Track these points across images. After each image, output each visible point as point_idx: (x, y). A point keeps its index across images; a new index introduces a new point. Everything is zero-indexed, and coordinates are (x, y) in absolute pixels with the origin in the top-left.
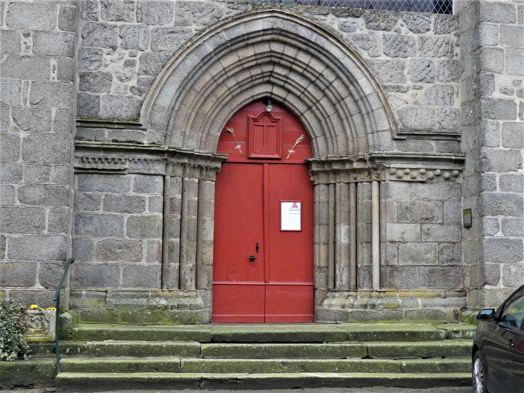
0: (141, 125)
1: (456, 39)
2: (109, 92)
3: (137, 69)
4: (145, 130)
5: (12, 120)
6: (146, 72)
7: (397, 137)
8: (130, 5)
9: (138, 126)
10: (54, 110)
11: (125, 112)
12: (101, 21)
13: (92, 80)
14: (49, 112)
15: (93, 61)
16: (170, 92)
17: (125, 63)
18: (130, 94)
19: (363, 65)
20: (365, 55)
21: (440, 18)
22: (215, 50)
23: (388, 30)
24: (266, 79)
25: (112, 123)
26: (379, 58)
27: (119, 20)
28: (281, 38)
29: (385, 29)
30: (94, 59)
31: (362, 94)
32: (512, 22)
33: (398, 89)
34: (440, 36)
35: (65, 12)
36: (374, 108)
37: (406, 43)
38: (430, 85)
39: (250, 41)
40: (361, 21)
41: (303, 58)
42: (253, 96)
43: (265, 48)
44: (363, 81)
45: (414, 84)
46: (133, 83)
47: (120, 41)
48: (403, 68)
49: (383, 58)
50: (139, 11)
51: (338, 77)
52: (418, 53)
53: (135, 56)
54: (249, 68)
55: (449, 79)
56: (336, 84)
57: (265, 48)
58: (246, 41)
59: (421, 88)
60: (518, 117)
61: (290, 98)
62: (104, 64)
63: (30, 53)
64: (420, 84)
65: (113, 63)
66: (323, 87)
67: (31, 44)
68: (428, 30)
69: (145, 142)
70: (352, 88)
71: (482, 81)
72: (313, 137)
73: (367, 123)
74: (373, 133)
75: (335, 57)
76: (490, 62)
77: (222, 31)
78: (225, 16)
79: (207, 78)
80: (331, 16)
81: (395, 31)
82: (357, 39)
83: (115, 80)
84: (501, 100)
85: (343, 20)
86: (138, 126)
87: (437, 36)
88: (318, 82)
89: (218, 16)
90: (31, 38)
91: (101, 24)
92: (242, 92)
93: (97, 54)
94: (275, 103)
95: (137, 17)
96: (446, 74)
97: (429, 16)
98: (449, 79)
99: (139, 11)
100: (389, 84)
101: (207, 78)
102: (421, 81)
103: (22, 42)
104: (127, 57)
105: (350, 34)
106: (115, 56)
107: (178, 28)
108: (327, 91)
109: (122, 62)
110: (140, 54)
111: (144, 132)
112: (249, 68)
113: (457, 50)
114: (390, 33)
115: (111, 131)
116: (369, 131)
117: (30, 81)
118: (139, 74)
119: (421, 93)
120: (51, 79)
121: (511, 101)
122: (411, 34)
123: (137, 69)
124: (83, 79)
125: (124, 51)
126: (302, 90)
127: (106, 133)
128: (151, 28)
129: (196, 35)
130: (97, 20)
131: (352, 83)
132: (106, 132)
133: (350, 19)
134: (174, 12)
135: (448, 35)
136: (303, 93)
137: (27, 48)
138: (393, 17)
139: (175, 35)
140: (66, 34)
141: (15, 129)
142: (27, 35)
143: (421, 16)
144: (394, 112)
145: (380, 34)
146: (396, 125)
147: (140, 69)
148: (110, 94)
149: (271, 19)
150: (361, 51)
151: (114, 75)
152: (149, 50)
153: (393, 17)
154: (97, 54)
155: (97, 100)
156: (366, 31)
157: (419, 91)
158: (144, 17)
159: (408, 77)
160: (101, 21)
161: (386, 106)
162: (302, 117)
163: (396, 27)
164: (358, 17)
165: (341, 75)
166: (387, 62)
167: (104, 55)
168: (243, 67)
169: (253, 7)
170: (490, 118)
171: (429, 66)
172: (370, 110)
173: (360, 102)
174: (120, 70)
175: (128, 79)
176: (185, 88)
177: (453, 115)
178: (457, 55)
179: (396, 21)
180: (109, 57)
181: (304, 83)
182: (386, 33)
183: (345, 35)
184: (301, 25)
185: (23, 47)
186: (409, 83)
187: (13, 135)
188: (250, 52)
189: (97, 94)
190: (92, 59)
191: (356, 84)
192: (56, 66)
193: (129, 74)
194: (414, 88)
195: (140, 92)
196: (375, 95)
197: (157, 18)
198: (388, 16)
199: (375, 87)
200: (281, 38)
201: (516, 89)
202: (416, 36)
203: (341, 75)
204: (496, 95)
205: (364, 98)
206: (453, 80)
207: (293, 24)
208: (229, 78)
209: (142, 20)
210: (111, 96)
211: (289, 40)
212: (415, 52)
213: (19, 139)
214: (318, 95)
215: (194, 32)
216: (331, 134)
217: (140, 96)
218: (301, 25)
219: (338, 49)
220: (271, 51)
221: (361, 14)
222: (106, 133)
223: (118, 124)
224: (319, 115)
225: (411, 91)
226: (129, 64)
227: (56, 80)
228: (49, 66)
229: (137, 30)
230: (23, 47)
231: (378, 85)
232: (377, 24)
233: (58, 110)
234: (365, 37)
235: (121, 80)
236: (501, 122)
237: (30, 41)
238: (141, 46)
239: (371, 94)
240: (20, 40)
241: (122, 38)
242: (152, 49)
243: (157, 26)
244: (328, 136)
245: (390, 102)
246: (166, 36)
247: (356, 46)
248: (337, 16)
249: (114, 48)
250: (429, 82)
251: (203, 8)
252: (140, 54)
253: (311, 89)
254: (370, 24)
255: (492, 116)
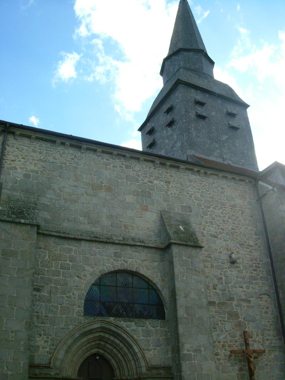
0: (51, 367)
1: (168, 330)
2: (38, 353)
3: (49, 343)
4: (53, 369)
5: (5, 367)
6: (53, 345)
7: (148, 369)
8: (47, 318)
9: (49, 367)
10: (22, 362)
11: (44, 362)
12: (36, 324)
13: (32, 348)
14: (20, 363)
15: (33, 340)
16: (62, 353)
17: (45, 341)
18: (46, 354)
19: (135, 340)
20: (135, 337)
21: (162, 322)
22: (79, 336)
23: (144, 327)
24: (97, 346)
25: (40, 366)
26: (140, 338)
27: (43, 324)
28: (104, 330)
29: (142, 326)
30: (33, 339)
31: (135, 352)
32: (189, 324)
33: (148, 350)
34: (163, 328)
35: (27, 323)
36: (139, 357)
37: (150, 332)
38: (159, 348)
39: (92, 332)
40: (133, 323)
41: (112, 338)
42: (91, 353)
43: (97, 334)
44: (135, 347)
45: (153, 347)
46: (48, 349)
47: (43, 332)
48: (149, 341)
49: (142, 338)
50: (50, 320)
51: (125, 345)
52: (155, 336)
53: (48, 338)
54: (91, 342)
55: (166, 345)
56: (124, 348)
57: (97, 334)
58: (91, 332)
59: (156, 349)
60: (193, 360)
61: (106, 354)
62: (36, 342)
63: (14, 339)
64: (156, 347)
65: (40, 341)
66: (119, 349)
67: (14, 336)
68: (158, 326)
69: (52, 374)
70: (131, 350)
71: (180, 347)
72: (115, 369)
73: (137, 363)
74: (139, 367)
75: (124, 338)
76: (182, 339)
77: (82, 328)
78: (83, 322)
79: (76, 347)
80: (123, 322)
81: (146, 327)
82: (132, 330)
83: (41, 348)
84: (187, 354)
85: (126, 323)
86: (49, 367)
87: (161, 328)
88: (117, 347)
89: (81, 322)
90: (14, 333)
91: (36, 326)
92: (87, 351)
93: (34, 337)
94: (99, 355)
95: (50, 323)
96: (165, 343)
97: (158, 321)
98: (166, 345)
99: (50, 320)
100: (145, 348)
101: (76, 347)
102: (156, 346)
103: (10, 335)
104: (45, 339)
105: (130, 328)
106: (41, 338)
107: (65, 327)
108: (121, 351)
109: (43, 341)
110: (50, 337)
111: (52, 370)
112: (91, 342)
113: (169, 334)
114: (144, 328)
115: (39, 369)
116: (138, 366)
117: (13, 351)
118: (50, 346)
119: (156, 351)
120: (21, 350)
121: (190, 354)
122: (152, 328)
123: (49, 343)
124: (31, 348)
125: (44, 336)
126: (111, 350)
127: (37, 370)
128: (55, 327)
129: (72, 330)
130: (34, 324)
131: (131, 348)
132: (37, 370)
133: (129, 323)
134: (64, 321)
135: (165, 328)
136: (111, 352)
137: (12, 337)
138: (145, 322)
139: (64, 330)
140: (27, 332)
141: (7, 371)
142: (12, 332)
143: (155, 321)
144: (147, 359)
145: (140, 328)
146: (148, 364)
147: (50, 344)
148: (39, 354)
149: (101, 323)
150: (134, 335)
151: (40, 346)
152: (54, 336)
153: (145, 322)
154: (34, 337)
155: (33, 357)
156: (135, 327)
157: (155, 350)
158: (53, 322)
159: (151, 345)
160: (36, 324)
161: (144, 357)
162: (110, 361)
163: (146, 326)
164: (132, 322)
165: (127, 345)
166: (144, 339)
167: (37, 338)
168: (89, 342)
169: (94, 319)
170: (183, 361)
171: (159, 340)
172: (138, 358)
173: (134, 355)
174: (43, 344)
175: (46, 348)
176: (67, 352)
177: (168, 359)
178: (168, 336)
179: (146, 323)
180: (38, 339)
181: (111, 348)
182: (143, 328)
183: (128, 329)
184: (112, 325)
185: (11, 337)
186: (152, 347)
187: (6, 373)
188: (92, 336)
189: (34, 354)
190: (32, 340)
191: (132, 348)
192: (23, 344)
193: (46, 346)
194: (154, 349)
195: (50, 353)
196: (139, 353)
197: (57, 324)
198: (143, 321)
199: (140, 349)
200: (104, 330)
201: (192, 349)
202: (153, 329)
203: (127, 345)
204: (185, 352)
205: (136, 354)
206: (167, 345)
207: (109, 325)
208: (83, 346)
209: (51, 324)
210: (39, 355)
211: (132, 339)
212: (153, 335)
213: (8, 375)
214: (117, 352)
215: (72, 329)
216: (122, 368)
217: (51, 355)
218: (112, 325)
219: (125, 335)
220: (100, 335)
221: (133, 321)
222: (37, 370)
223: (42, 367)
224: (117, 360)
225: (153, 351)
226: (46, 342)
227: (23, 350)
228: (20, 344)
229: (50, 328)
230: (11, 337)
231: (141, 348)
232: (139, 324)
233: (23, 362)
234: (135, 330)
235: (43, 348)
236: (187, 362)
237: (13, 334)
238: (51, 334)
239: (138, 352)
240: (10, 334)
241: (43, 331)
242: (55, 336)
243: (57, 326)
244: (121, 369)
245: (145, 355)
246: (61, 330)
247: (132, 333)
248: (125, 322)
249: (40, 335)
250: (159, 347)
251: (75, 319)
252: (50, 337)
253: (114, 350)
254: (137, 324)
255: (184, 361)
